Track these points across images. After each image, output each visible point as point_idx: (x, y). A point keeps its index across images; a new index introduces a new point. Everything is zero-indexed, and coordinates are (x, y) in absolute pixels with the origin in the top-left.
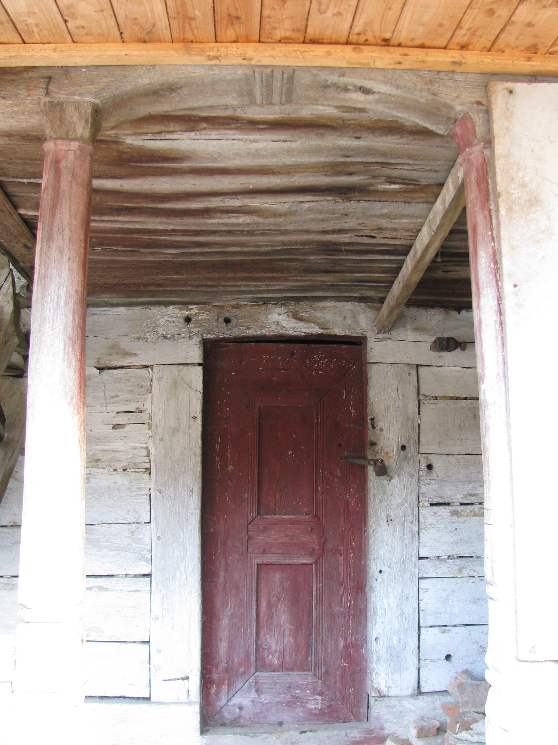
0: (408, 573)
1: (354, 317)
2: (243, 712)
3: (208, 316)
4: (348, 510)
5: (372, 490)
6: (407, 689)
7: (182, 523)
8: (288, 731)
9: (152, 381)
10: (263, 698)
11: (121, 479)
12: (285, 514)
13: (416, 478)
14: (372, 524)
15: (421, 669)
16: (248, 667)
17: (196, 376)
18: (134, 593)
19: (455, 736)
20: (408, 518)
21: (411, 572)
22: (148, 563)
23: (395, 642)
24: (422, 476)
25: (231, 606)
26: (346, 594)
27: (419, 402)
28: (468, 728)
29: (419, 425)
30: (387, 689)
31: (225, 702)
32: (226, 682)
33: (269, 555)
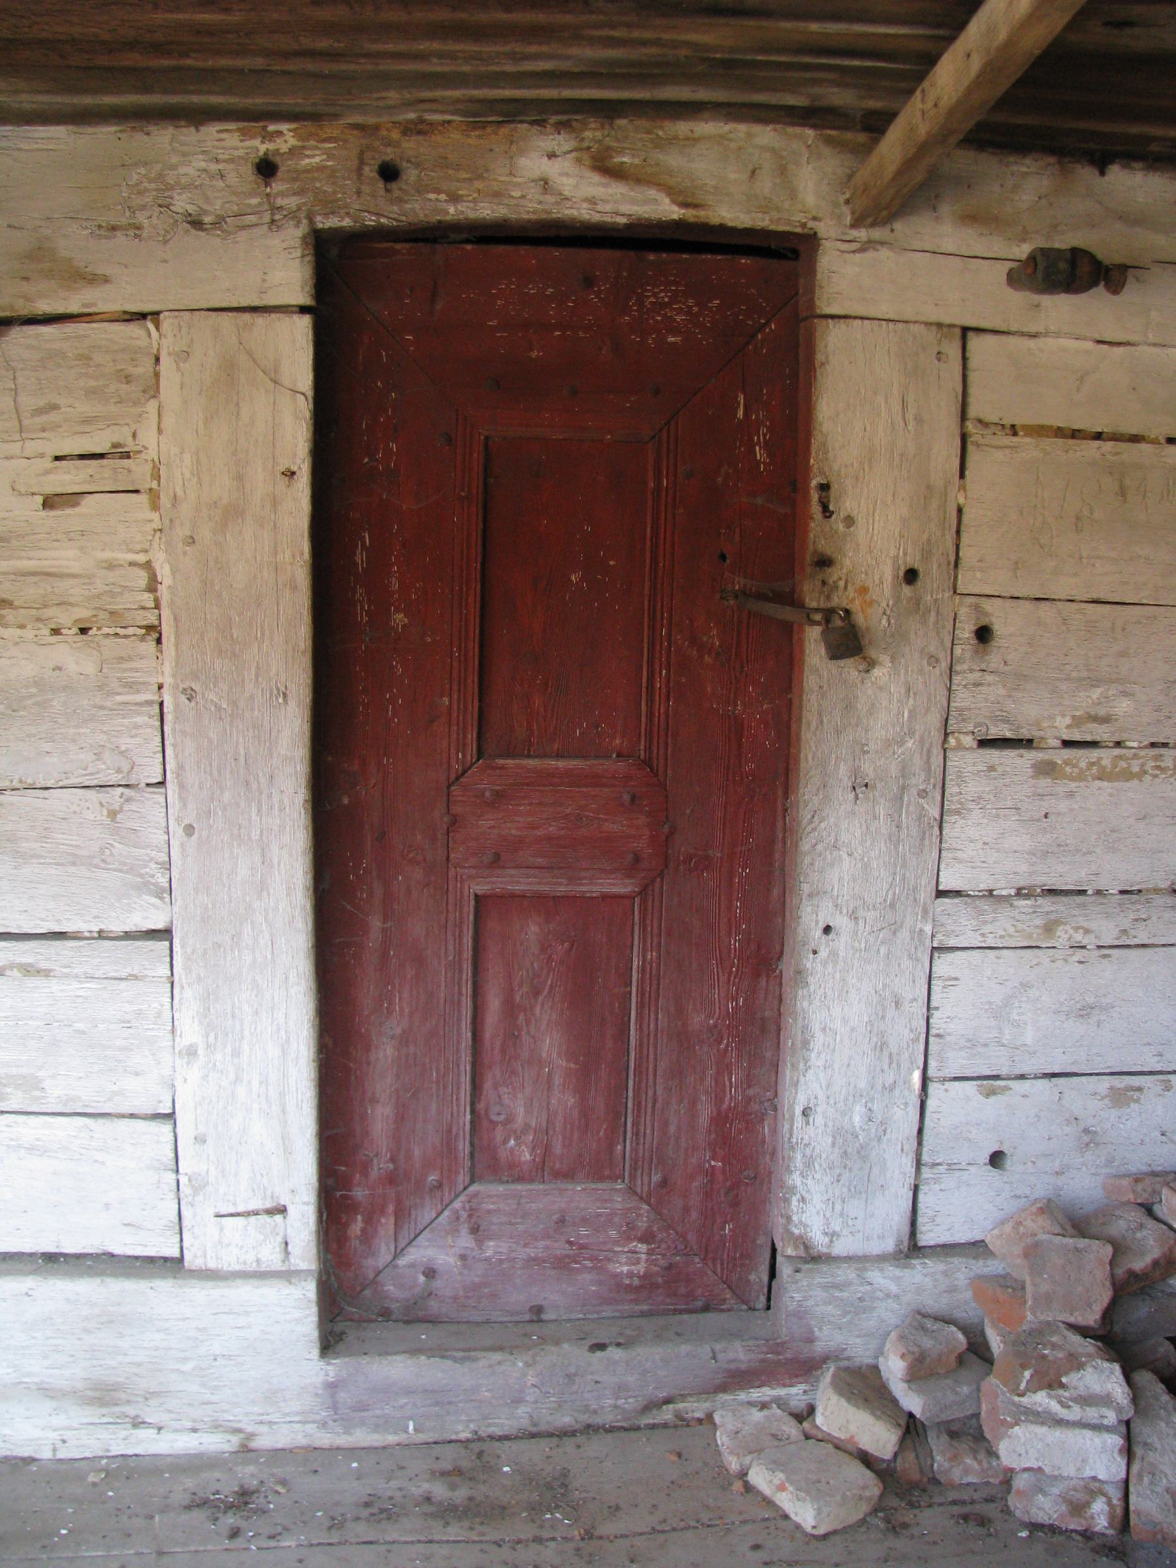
0: (904, 934)
1: (782, 171)
2: (438, 1283)
3: (330, 157)
4: (740, 745)
5: (814, 697)
6: (881, 1237)
7: (255, 786)
8: (557, 1343)
9: (157, 360)
10: (491, 1248)
11: (75, 660)
12: (558, 756)
13: (944, 664)
14: (808, 794)
15: (923, 1189)
16: (450, 1170)
17: (293, 347)
18: (123, 984)
19: (1016, 1399)
20: (913, 781)
21: (912, 931)
22: (161, 898)
23: (857, 1119)
24: (961, 660)
25: (402, 1009)
26: (724, 978)
27: (964, 438)
28: (1053, 1384)
29: (960, 511)
30: (827, 1239)
31: (389, 1258)
32: (391, 1208)
33: (513, 872)
